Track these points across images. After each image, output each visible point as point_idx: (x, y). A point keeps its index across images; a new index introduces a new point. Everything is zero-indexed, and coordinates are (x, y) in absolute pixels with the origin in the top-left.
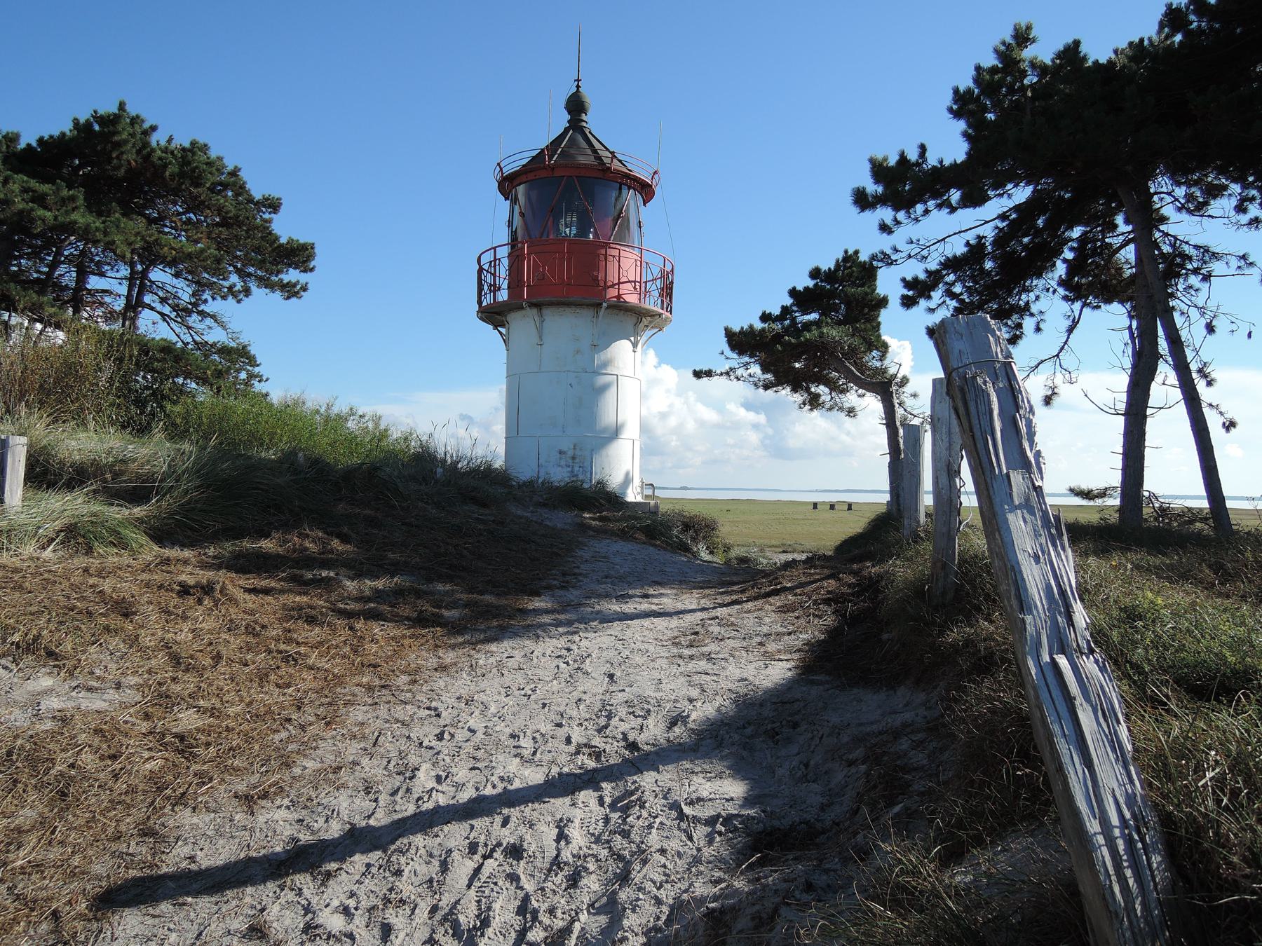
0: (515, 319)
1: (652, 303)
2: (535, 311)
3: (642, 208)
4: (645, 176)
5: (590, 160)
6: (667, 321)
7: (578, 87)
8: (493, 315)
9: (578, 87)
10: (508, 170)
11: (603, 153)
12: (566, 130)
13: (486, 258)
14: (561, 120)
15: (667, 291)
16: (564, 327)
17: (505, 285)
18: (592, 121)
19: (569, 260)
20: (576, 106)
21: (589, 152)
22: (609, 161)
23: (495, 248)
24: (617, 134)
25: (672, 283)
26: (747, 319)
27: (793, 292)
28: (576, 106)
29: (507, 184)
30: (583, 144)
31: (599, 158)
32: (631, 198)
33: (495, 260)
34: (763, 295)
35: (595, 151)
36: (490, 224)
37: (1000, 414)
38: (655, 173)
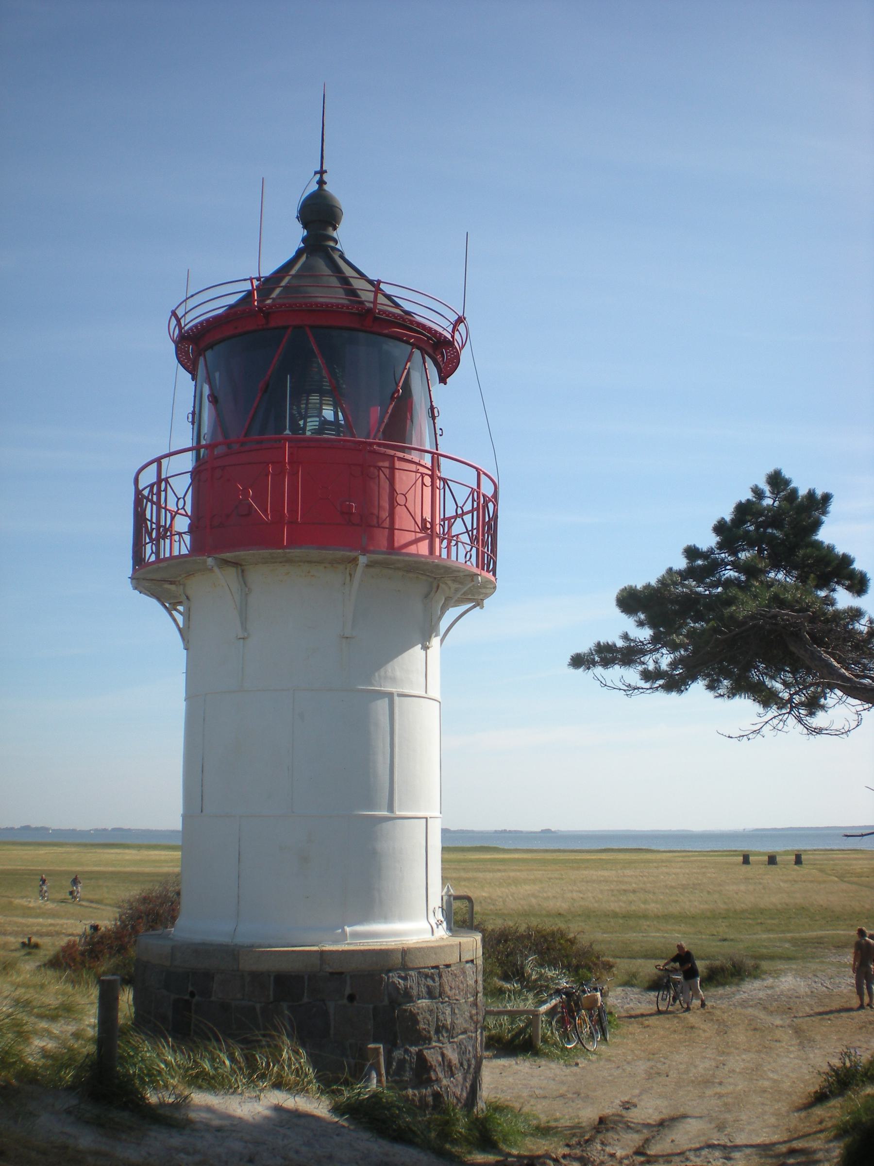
0: (198, 587)
1: (462, 555)
2: (232, 572)
3: (437, 389)
4: (442, 325)
5: (338, 297)
6: (489, 588)
7: (321, 182)
8: (155, 578)
9: (321, 182)
10: (191, 320)
11: (358, 284)
12: (299, 253)
13: (149, 477)
14: (290, 238)
15: (486, 533)
16: (293, 604)
17: (182, 524)
18: (348, 238)
19: (294, 475)
20: (319, 214)
21: (334, 282)
22: (371, 296)
23: (158, 461)
24: (391, 253)
25: (495, 517)
26: (646, 575)
27: (692, 553)
28: (319, 214)
29: (196, 344)
30: (325, 270)
31: (352, 292)
32: (421, 373)
33: (159, 480)
34: (671, 527)
35: (345, 281)
36: (159, 418)
37: (285, 417)
38: (460, 320)
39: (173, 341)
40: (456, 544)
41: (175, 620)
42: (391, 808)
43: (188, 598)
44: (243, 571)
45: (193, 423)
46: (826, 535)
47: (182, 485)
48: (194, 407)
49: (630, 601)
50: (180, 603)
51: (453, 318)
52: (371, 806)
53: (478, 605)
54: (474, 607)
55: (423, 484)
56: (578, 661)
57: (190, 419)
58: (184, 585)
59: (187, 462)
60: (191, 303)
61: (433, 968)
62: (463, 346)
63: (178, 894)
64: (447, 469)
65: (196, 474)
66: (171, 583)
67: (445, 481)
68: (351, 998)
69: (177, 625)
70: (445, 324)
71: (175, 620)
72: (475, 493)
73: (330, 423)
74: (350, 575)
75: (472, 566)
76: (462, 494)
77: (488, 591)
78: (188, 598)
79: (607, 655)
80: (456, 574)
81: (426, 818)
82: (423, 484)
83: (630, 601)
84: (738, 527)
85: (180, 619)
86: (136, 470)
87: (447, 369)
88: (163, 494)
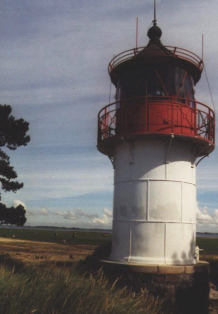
6: (212, 148)
13: (103, 113)
15: (211, 132)
42: (147, 219)
47: (112, 115)
51: (199, 61)
52: (142, 218)
59: (113, 107)
60: (115, 59)
63: (202, 62)
64: (198, 107)
65: (116, 115)
67: (199, 111)
70: (197, 63)
72: (209, 115)
75: (207, 140)
76: (205, 116)
81: (165, 223)
85: (112, 160)
86: (98, 113)
87: (197, 78)
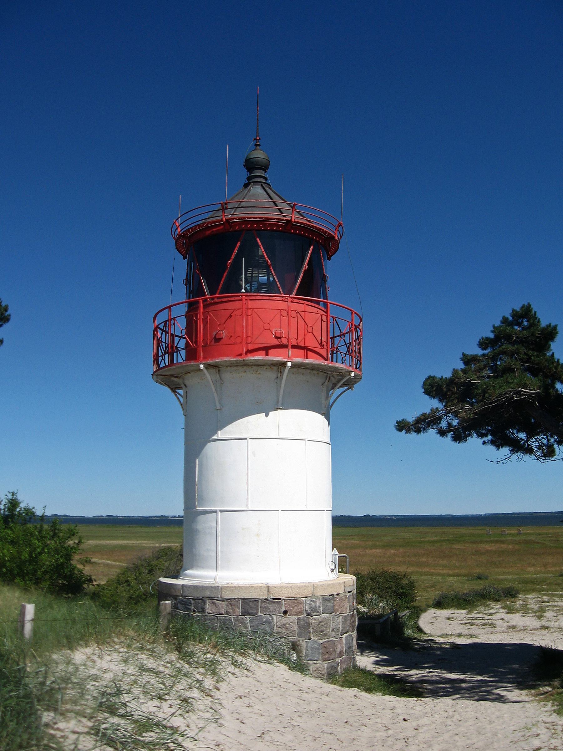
13: (164, 316)
23: (169, 308)
39: (174, 238)
40: (337, 353)
41: (178, 398)
43: (185, 385)
44: (219, 371)
45: (186, 285)
46: (264, 414)
48: (187, 276)
49: (433, 388)
50: (180, 388)
53: (350, 388)
54: (348, 389)
55: (322, 320)
56: (402, 426)
57: (185, 283)
58: (183, 379)
61: (330, 595)
62: (341, 238)
66: (176, 377)
68: (285, 613)
69: (180, 402)
71: (178, 398)
73: (264, 284)
74: (281, 372)
77: (357, 380)
78: (185, 385)
79: (420, 425)
80: (341, 371)
82: (322, 320)
83: (433, 388)
84: (154, 595)
88: (173, 327)
